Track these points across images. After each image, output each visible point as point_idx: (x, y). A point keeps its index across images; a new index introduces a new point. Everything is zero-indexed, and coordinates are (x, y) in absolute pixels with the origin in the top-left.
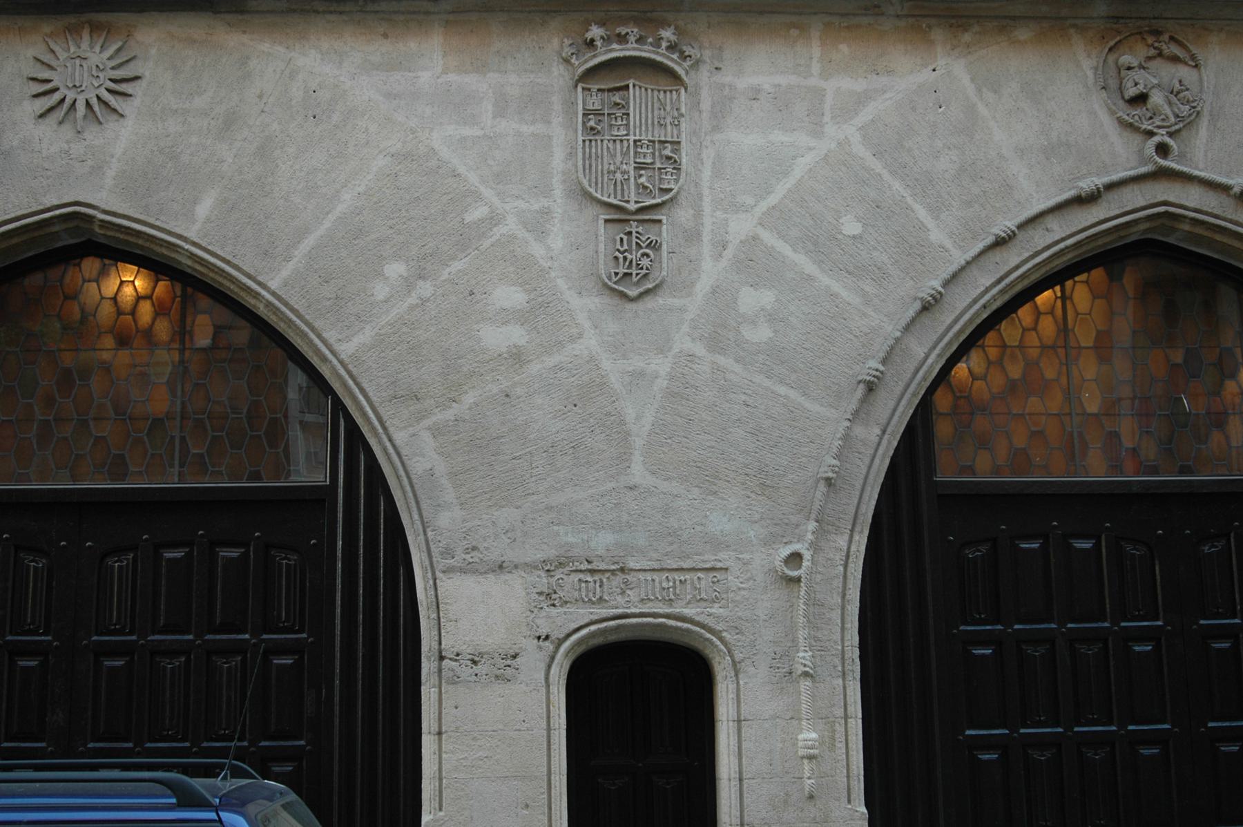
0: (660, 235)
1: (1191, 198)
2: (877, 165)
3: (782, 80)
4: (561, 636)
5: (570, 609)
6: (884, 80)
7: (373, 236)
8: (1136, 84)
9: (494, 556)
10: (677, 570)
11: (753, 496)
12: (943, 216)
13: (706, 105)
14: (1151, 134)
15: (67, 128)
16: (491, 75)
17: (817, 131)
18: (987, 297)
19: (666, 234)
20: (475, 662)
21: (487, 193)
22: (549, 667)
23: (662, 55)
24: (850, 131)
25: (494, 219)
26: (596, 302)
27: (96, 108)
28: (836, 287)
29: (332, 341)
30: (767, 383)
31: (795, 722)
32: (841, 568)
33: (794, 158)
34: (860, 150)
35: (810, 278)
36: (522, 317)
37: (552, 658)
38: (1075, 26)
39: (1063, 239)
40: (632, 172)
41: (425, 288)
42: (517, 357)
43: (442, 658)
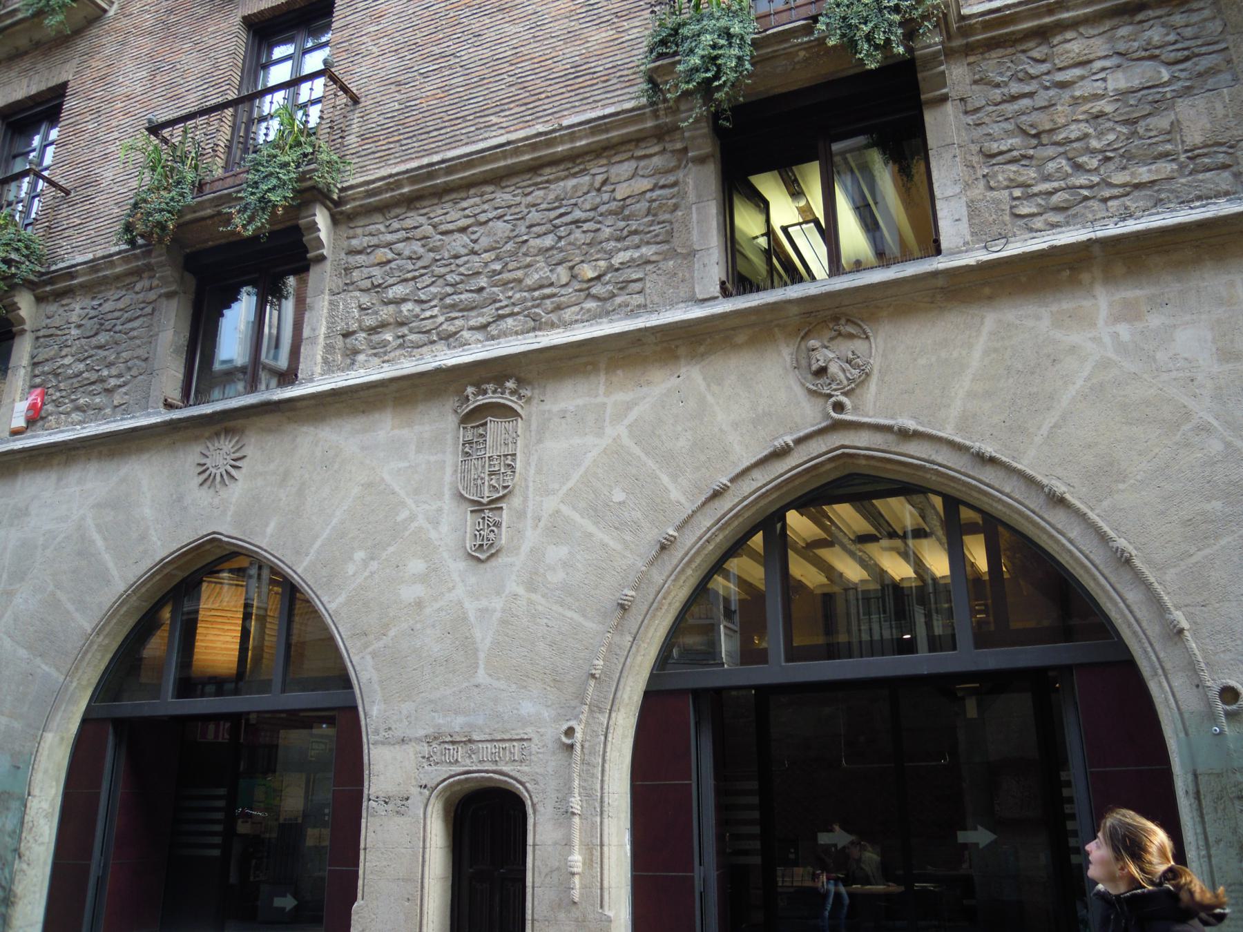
0: (501, 517)
1: (861, 440)
2: (637, 451)
3: (580, 402)
4: (433, 785)
5: (438, 767)
6: (645, 389)
7: (350, 536)
8: (818, 361)
9: (399, 734)
10: (500, 740)
11: (549, 688)
12: (679, 480)
13: (534, 426)
14: (830, 396)
15: (212, 490)
16: (416, 427)
17: (600, 433)
18: (708, 535)
19: (505, 516)
20: (386, 803)
21: (409, 502)
22: (426, 806)
23: (506, 399)
24: (622, 430)
25: (412, 518)
26: (462, 565)
27: (225, 477)
28: (607, 539)
29: (325, 603)
30: (561, 610)
31: (567, 847)
32: (603, 738)
33: (585, 453)
34: (627, 441)
35: (590, 535)
36: (423, 579)
37: (428, 800)
38: (778, 326)
39: (765, 485)
40: (487, 478)
41: (374, 565)
42: (419, 604)
43: (369, 800)
